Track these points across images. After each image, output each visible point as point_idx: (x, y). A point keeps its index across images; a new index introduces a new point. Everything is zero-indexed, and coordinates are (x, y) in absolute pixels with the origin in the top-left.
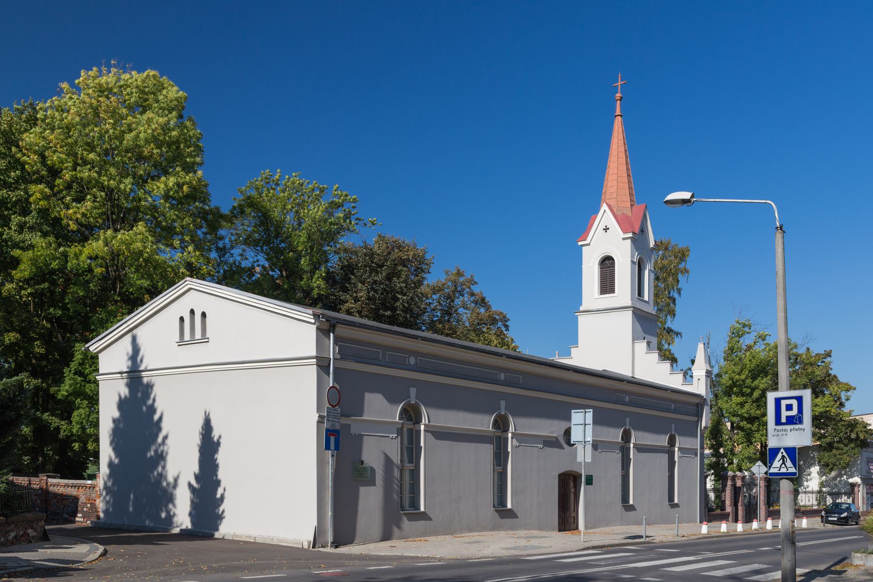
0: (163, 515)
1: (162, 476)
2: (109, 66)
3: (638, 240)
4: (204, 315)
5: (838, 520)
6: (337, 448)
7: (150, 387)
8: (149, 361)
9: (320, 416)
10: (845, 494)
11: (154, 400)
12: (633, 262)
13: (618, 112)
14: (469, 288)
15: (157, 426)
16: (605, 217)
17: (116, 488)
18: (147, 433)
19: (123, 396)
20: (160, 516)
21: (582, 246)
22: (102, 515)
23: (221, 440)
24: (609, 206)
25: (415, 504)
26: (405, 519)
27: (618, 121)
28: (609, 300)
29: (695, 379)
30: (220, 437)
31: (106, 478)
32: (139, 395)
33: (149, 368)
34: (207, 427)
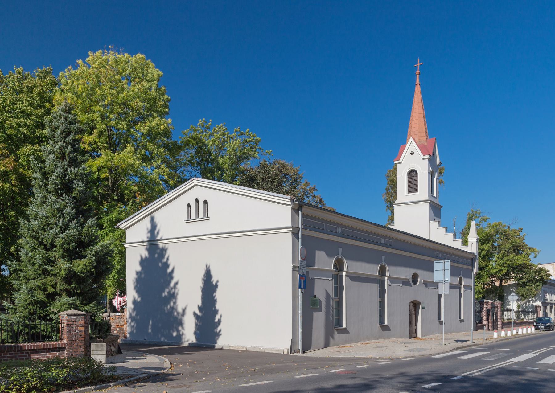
0: (175, 334)
1: (173, 309)
2: (108, 50)
3: (432, 160)
4: (205, 202)
5: (544, 328)
6: (305, 288)
7: (164, 250)
8: (163, 233)
9: (294, 267)
10: (532, 312)
11: (168, 259)
12: (429, 173)
13: (418, 82)
14: (312, 193)
15: (170, 276)
16: (411, 145)
17: (138, 317)
18: (162, 281)
19: (144, 257)
20: (172, 335)
21: (396, 164)
22: (128, 335)
23: (218, 284)
24: (414, 139)
25: (339, 323)
26: (336, 332)
27: (418, 89)
28: (413, 197)
29: (470, 244)
30: (218, 282)
31: (131, 311)
32: (156, 256)
33: (163, 238)
34: (208, 275)
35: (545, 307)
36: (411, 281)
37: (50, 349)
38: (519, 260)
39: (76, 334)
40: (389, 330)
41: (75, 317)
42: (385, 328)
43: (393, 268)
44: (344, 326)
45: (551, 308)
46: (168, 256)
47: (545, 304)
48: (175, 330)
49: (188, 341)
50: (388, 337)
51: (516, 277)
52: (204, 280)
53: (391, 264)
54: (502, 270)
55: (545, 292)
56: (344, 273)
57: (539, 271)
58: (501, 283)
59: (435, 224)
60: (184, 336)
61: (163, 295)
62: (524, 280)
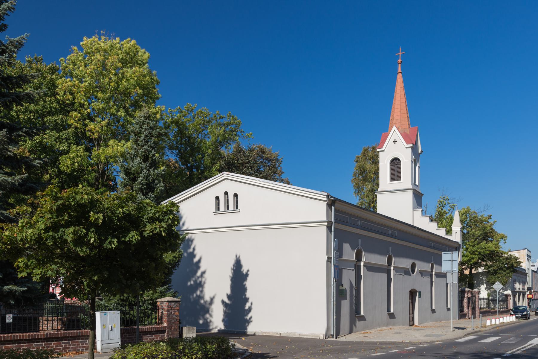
0: (201, 322)
1: (201, 297)
2: (99, 35)
3: (414, 149)
4: (236, 195)
7: (191, 241)
11: (194, 249)
13: (399, 71)
15: (197, 265)
16: (395, 134)
21: (379, 152)
23: (249, 273)
25: (358, 311)
27: (400, 77)
28: (396, 185)
30: (248, 271)
33: (190, 228)
34: (238, 265)
35: (514, 296)
36: (410, 270)
37: (155, 331)
38: (491, 246)
39: (174, 319)
40: (365, 320)
41: (173, 304)
42: (392, 316)
43: (398, 259)
44: (362, 313)
45: (519, 296)
46: (195, 246)
47: (514, 293)
48: (201, 318)
49: (216, 328)
50: (394, 325)
51: (486, 265)
52: (233, 269)
53: (397, 256)
54: (473, 258)
55: (514, 281)
56: (362, 264)
57: (510, 258)
58: (471, 271)
59: (418, 212)
60: (211, 324)
61: (189, 284)
62: (495, 268)
